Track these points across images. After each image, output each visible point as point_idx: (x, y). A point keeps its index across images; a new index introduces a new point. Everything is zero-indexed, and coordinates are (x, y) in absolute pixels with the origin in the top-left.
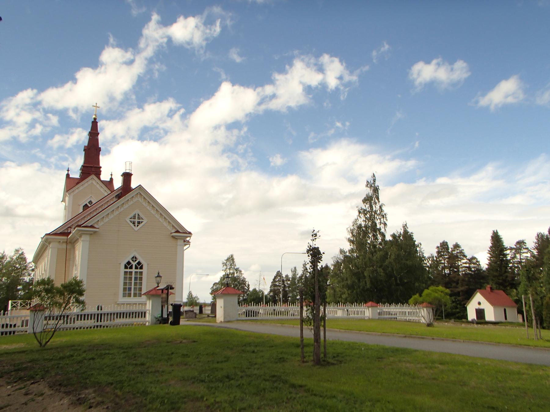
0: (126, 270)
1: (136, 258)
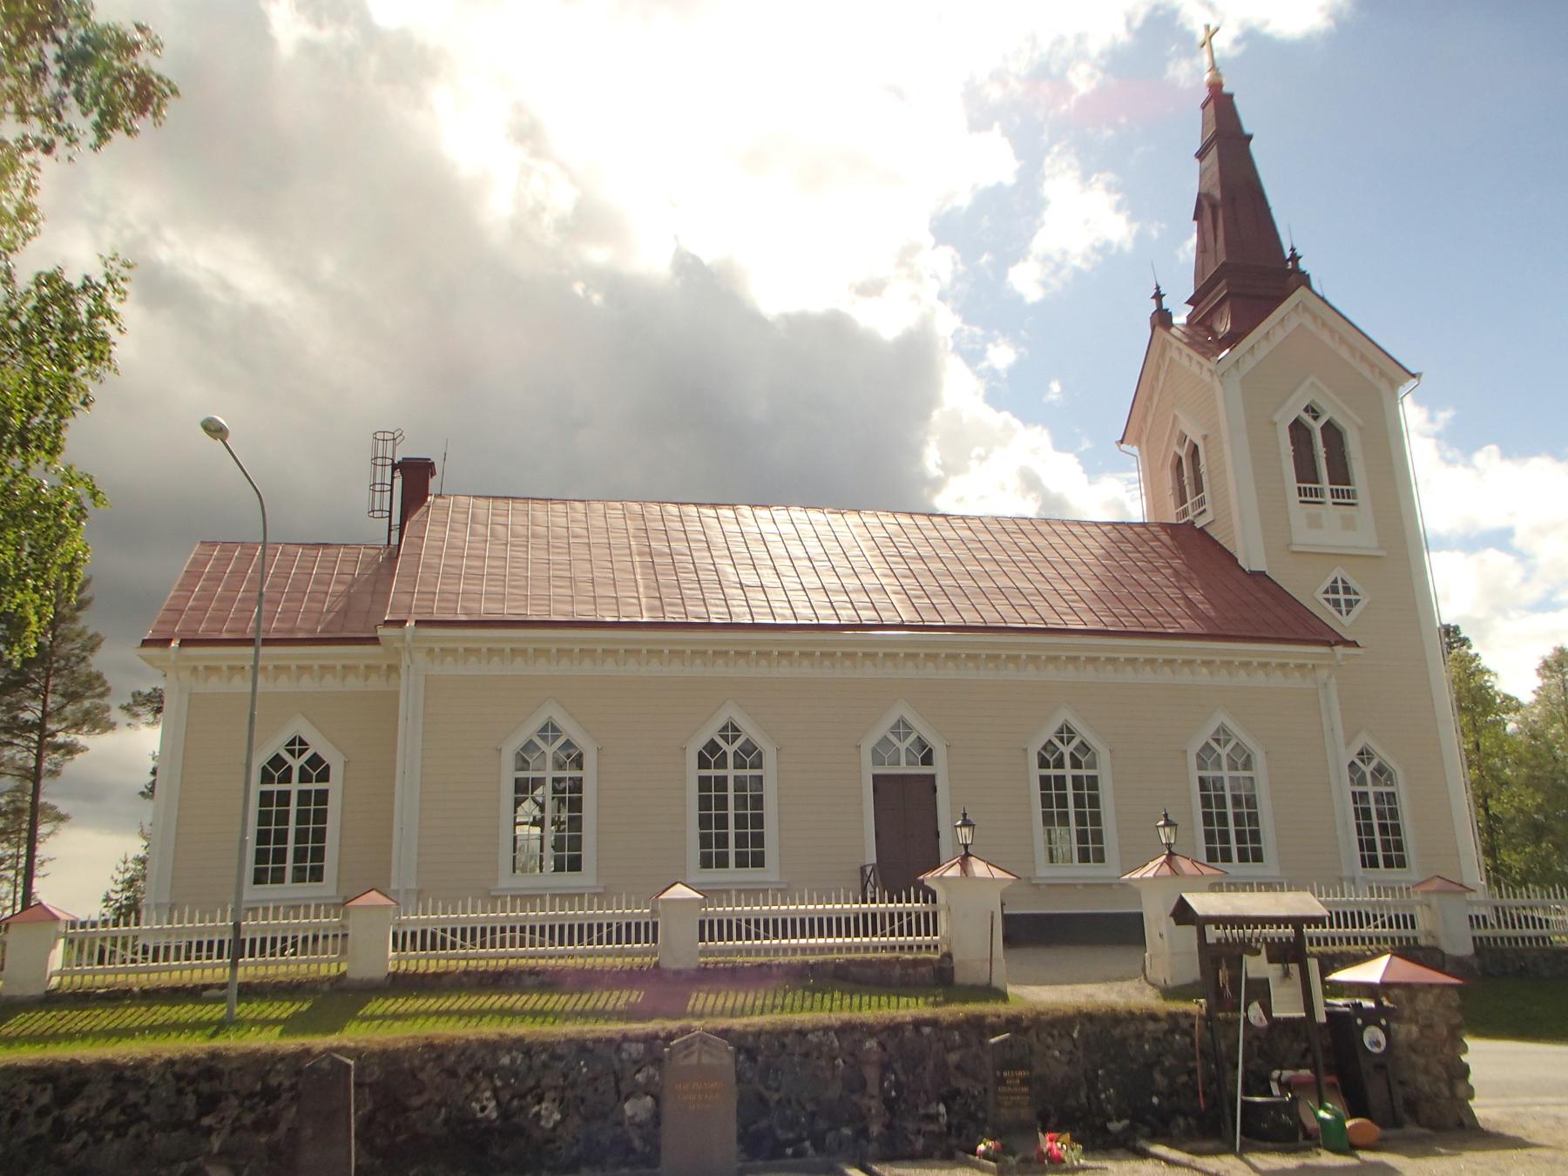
0: (705, 773)
1: (302, 742)
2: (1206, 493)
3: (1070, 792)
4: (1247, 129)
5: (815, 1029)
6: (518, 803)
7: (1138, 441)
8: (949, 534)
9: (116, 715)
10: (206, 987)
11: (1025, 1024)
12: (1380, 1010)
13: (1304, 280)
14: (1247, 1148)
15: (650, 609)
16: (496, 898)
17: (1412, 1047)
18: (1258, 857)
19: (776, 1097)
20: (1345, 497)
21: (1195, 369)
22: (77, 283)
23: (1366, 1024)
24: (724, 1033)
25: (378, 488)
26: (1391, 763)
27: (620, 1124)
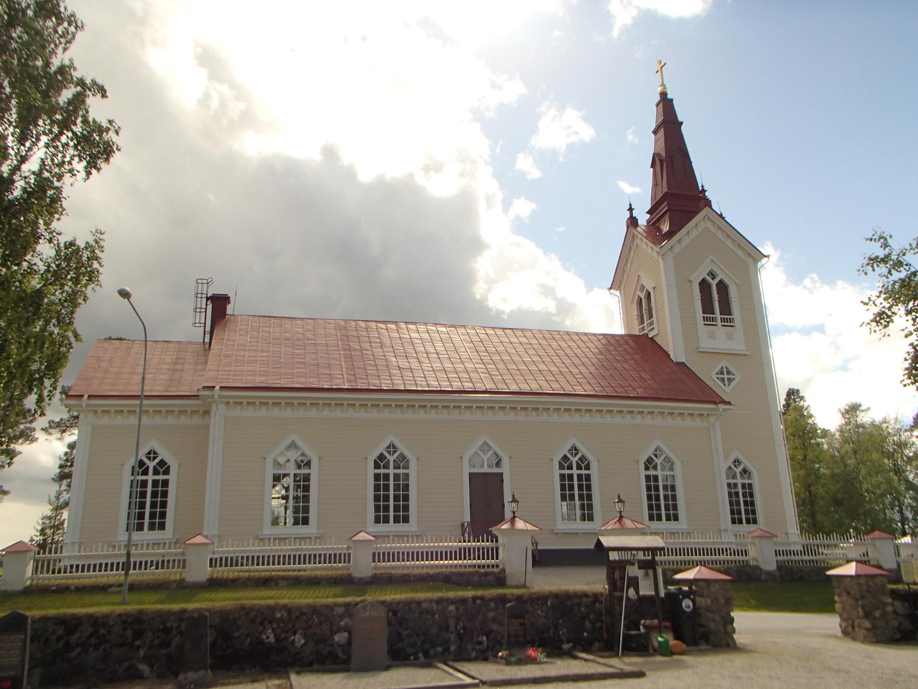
0: (378, 471)
1: (155, 453)
2: (654, 318)
3: (576, 483)
4: (680, 119)
5: (425, 601)
6: (274, 486)
7: (619, 288)
8: (514, 340)
9: (39, 434)
10: (110, 586)
11: (525, 598)
12: (691, 592)
13: (708, 203)
14: (623, 655)
15: (349, 381)
16: (263, 539)
17: (708, 610)
18: (676, 518)
19: (406, 633)
20: (728, 322)
21: (649, 250)
22: (82, 245)
23: (684, 597)
24: (383, 603)
25: (198, 310)
26: (750, 468)
27: (332, 645)
